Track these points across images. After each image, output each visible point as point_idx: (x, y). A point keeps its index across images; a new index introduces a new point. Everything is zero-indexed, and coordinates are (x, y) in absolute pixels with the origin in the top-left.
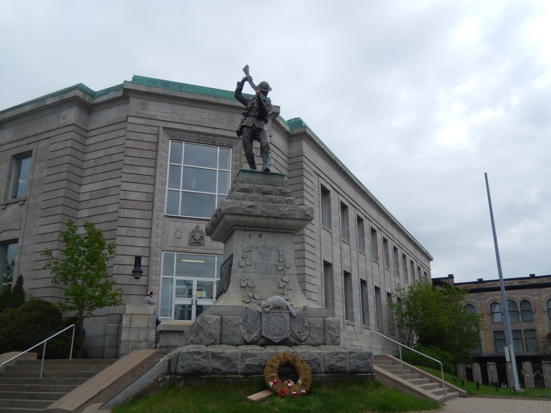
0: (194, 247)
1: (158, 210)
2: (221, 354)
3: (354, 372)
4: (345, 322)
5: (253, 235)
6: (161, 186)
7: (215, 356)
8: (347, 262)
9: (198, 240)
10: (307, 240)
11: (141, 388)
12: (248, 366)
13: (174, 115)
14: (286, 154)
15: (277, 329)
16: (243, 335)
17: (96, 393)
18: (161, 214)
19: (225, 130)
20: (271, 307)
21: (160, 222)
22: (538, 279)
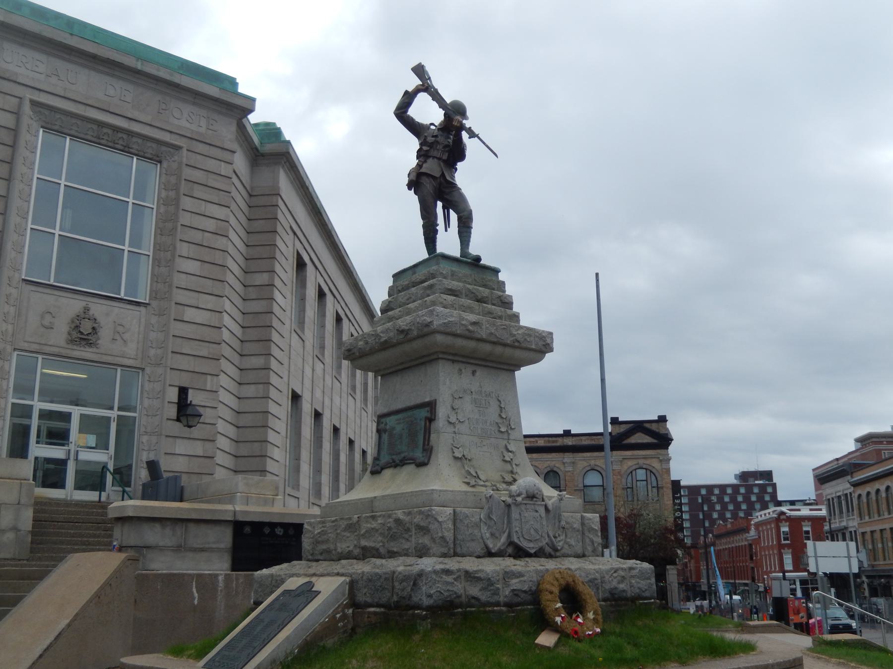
0: (78, 348)
2: (478, 574)
3: (634, 599)
4: (311, 501)
5: (477, 374)
6: (18, 220)
7: (470, 577)
8: (318, 394)
9: (85, 335)
10: (275, 351)
11: (310, 632)
12: (515, 592)
13: (54, 80)
14: (248, 188)
15: (532, 532)
16: (486, 540)
17: (52, 638)
18: (17, 275)
19: (151, 125)
22: (575, 438)
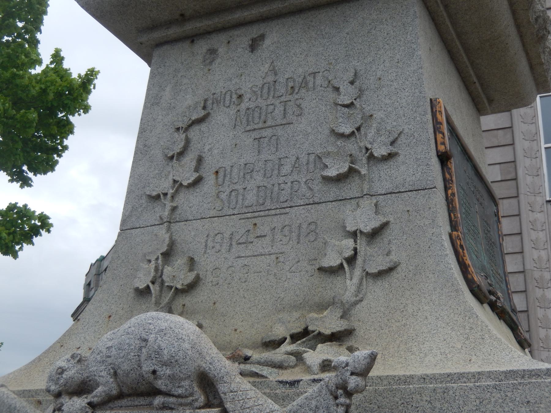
1: (529, 194)
5: (222, 51)
6: (527, 144)
18: (539, 199)
20: (100, 389)
21: (539, 216)
